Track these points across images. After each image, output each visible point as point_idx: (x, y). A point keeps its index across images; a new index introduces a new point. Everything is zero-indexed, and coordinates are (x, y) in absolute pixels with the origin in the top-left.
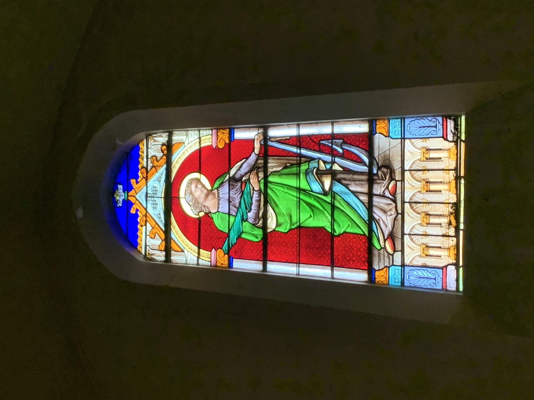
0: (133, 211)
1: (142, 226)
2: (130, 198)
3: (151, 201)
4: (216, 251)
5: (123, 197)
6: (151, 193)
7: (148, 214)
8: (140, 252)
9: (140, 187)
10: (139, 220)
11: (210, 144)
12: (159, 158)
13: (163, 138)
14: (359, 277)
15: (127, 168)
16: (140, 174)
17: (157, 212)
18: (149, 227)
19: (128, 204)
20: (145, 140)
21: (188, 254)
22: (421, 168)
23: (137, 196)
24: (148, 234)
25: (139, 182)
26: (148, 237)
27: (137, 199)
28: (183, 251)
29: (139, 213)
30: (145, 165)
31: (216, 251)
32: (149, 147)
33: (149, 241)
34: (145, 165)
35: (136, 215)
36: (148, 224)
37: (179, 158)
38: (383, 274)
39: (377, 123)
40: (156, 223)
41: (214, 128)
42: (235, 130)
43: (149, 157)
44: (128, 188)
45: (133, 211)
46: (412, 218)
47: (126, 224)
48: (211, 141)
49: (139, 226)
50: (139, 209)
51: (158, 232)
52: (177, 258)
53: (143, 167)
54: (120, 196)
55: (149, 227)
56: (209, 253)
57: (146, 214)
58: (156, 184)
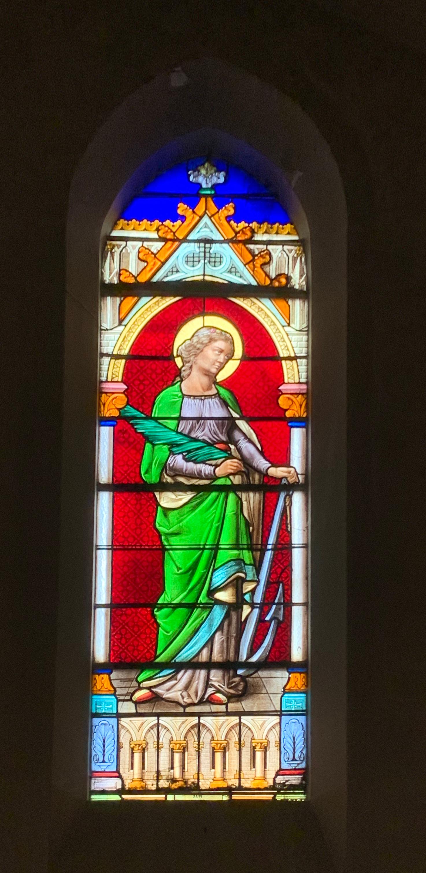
0: (182, 208)
1: (158, 230)
2: (203, 200)
3: (198, 250)
4: (123, 393)
5: (204, 186)
6: (212, 251)
7: (177, 243)
8: (114, 226)
9: (221, 225)
10: (168, 223)
11: (286, 381)
12: (267, 269)
13: (298, 281)
14: (100, 651)
15: (254, 201)
16: (243, 224)
17: (182, 266)
18: (156, 246)
19: (192, 195)
20: (296, 238)
21: (118, 331)
22: (160, 741)
23: (206, 219)
24: (146, 244)
25: (228, 222)
26: (140, 244)
27: (201, 217)
28: (120, 324)
29: (179, 222)
30: (258, 237)
31: (123, 393)
32: (286, 248)
33: (134, 247)
34: (258, 237)
35: (175, 217)
36: (161, 244)
37: (264, 311)
38: (105, 686)
39: (302, 675)
40: (163, 263)
41: (310, 386)
42: (304, 430)
43: (270, 247)
44: (220, 196)
45: (182, 208)
46: (180, 728)
47: (159, 198)
48: (291, 381)
49: (157, 223)
50: (186, 223)
51: (148, 269)
52: (109, 308)
53: (253, 232)
54: (207, 178)
55: (156, 246)
56: (120, 380)
57: (178, 240)
58: (225, 265)
